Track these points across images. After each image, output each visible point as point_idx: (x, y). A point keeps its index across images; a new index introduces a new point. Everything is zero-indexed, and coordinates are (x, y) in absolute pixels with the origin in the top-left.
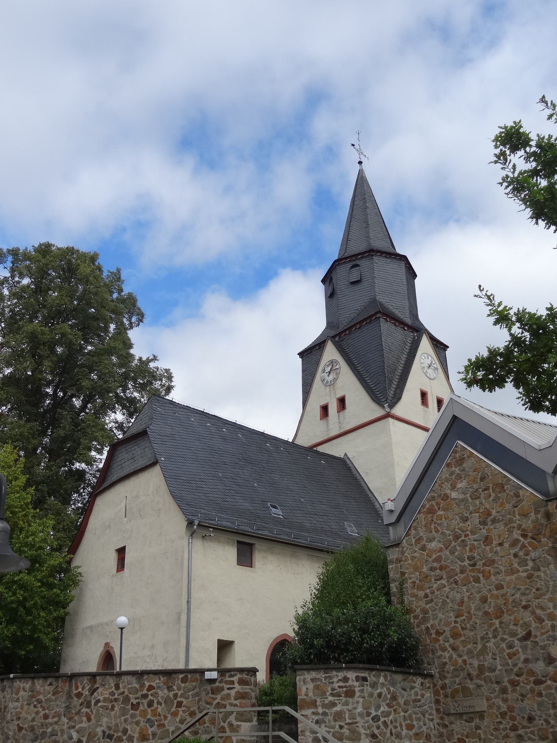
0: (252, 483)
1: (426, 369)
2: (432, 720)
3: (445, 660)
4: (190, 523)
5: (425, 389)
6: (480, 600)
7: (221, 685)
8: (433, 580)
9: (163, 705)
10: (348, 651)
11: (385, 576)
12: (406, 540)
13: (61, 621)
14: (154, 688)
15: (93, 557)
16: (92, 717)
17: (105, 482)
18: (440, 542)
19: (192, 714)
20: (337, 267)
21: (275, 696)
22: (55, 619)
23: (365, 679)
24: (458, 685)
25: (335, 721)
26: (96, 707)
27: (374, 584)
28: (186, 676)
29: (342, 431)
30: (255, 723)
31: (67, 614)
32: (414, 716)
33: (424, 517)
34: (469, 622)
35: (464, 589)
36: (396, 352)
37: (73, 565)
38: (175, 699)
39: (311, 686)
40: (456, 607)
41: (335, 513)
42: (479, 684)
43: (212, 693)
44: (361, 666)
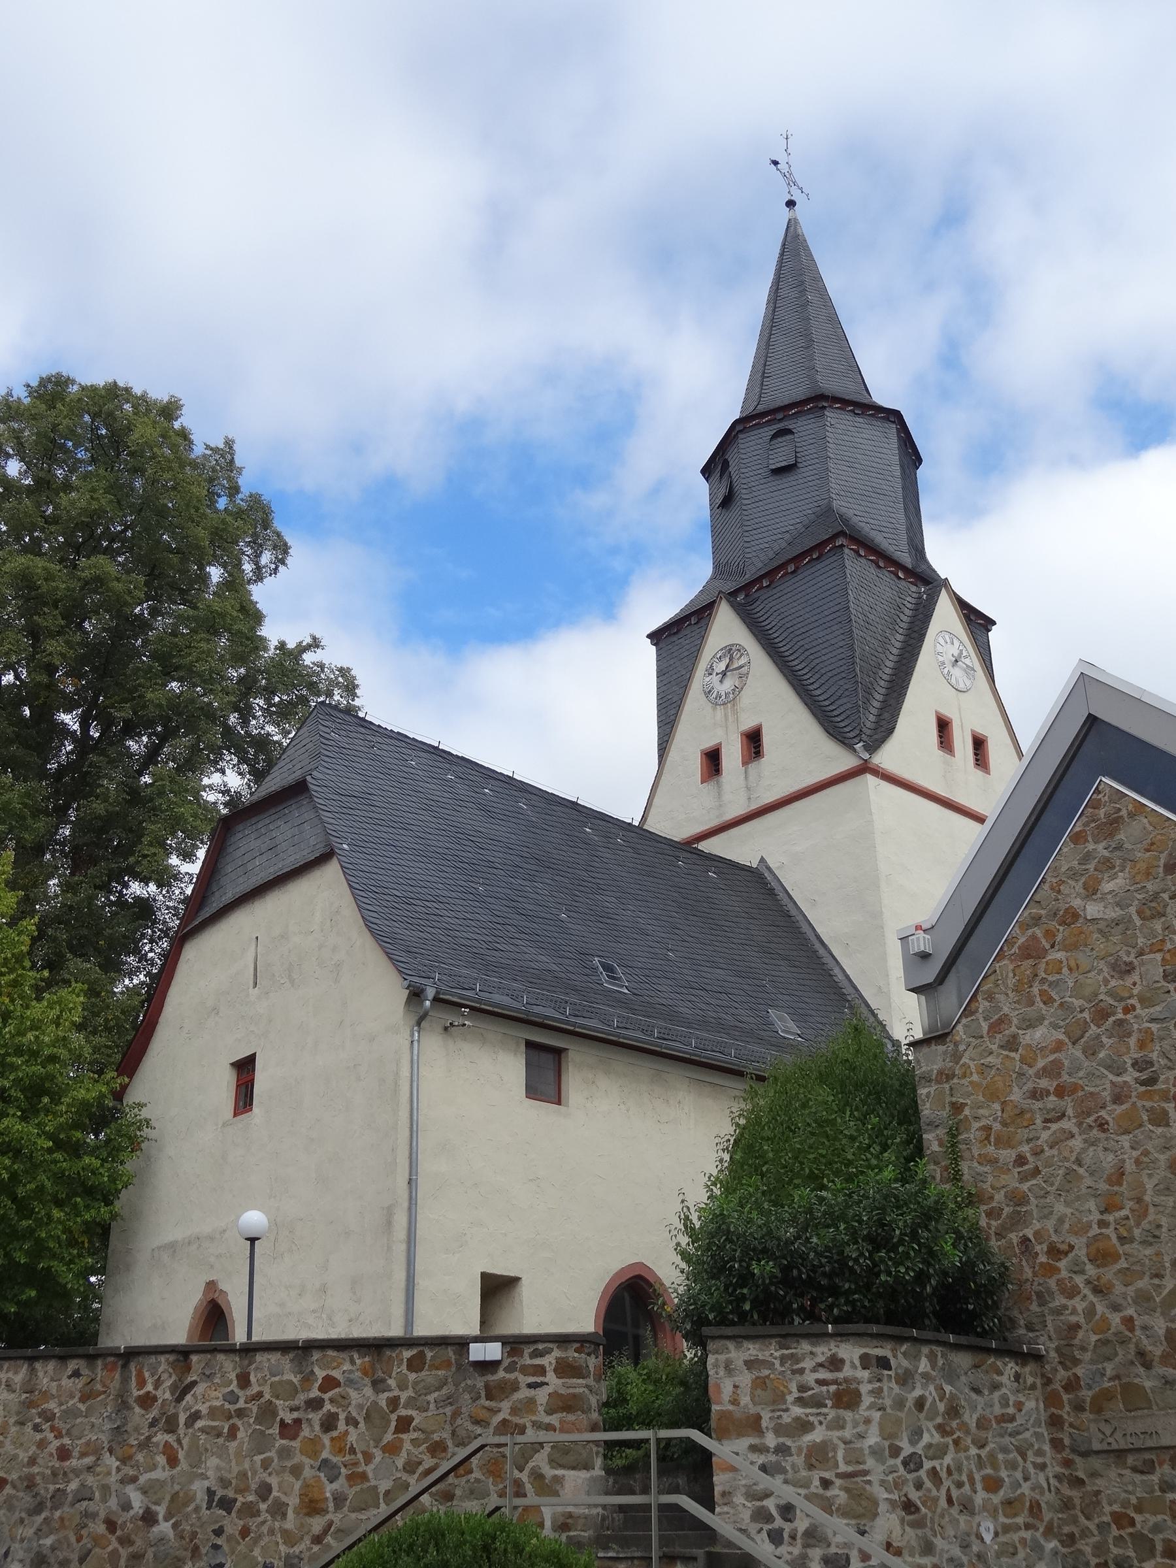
0: (554, 911)
1: (949, 667)
2: (1043, 1467)
3: (1073, 1319)
4: (415, 995)
5: (947, 712)
6: (1170, 1167)
7: (512, 1376)
8: (1038, 1121)
9: (362, 1425)
10: (834, 1291)
11: (909, 1115)
12: (965, 1026)
13: (101, 1233)
14: (337, 1384)
15: (178, 1082)
16: (181, 1455)
17: (202, 913)
18: (1055, 1026)
19: (437, 1449)
20: (741, 436)
21: (633, 1408)
22: (88, 1228)
23: (884, 1363)
24: (1110, 1379)
25: (811, 1467)
26: (190, 1430)
27: (880, 1133)
28: (421, 1355)
29: (754, 806)
30: (598, 1471)
31: (114, 1216)
32: (1000, 1456)
33: (1011, 967)
34: (1138, 1225)
35: (1125, 1141)
36: (880, 627)
37: (131, 1098)
38: (392, 1412)
39: (745, 1379)
40: (1103, 1186)
41: (746, 987)
42: (1170, 1379)
43: (489, 1397)
44: (875, 1329)
